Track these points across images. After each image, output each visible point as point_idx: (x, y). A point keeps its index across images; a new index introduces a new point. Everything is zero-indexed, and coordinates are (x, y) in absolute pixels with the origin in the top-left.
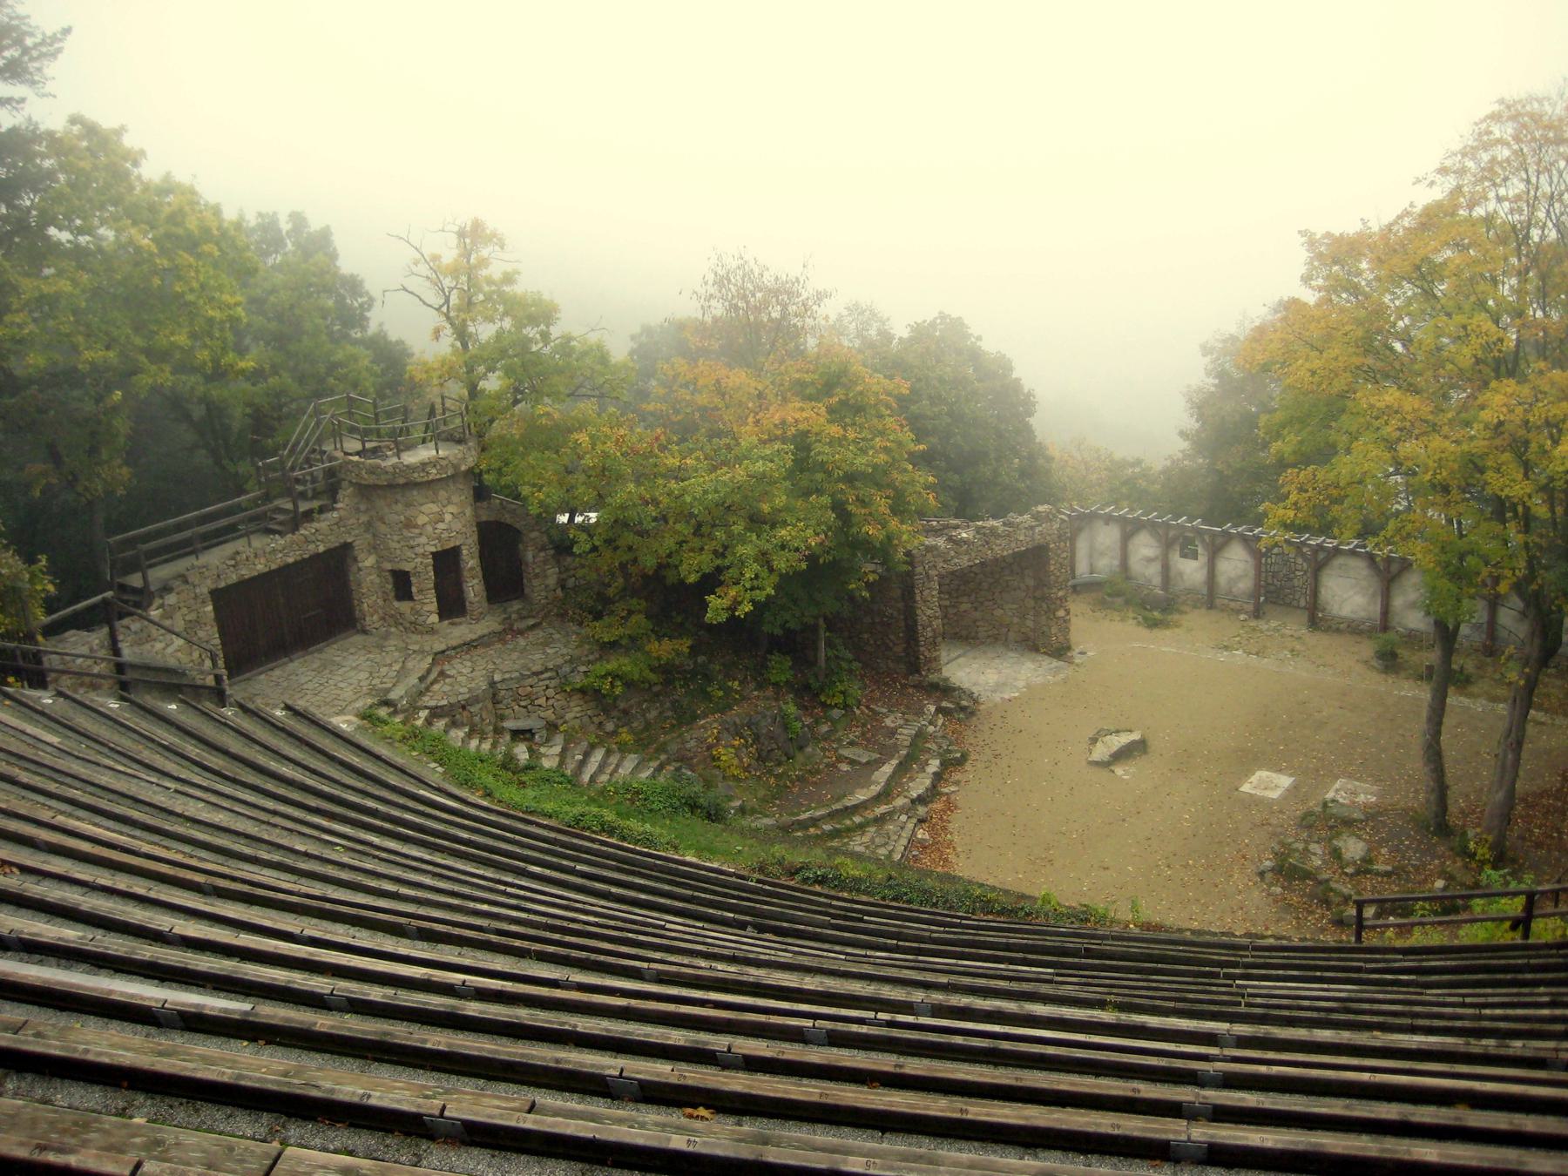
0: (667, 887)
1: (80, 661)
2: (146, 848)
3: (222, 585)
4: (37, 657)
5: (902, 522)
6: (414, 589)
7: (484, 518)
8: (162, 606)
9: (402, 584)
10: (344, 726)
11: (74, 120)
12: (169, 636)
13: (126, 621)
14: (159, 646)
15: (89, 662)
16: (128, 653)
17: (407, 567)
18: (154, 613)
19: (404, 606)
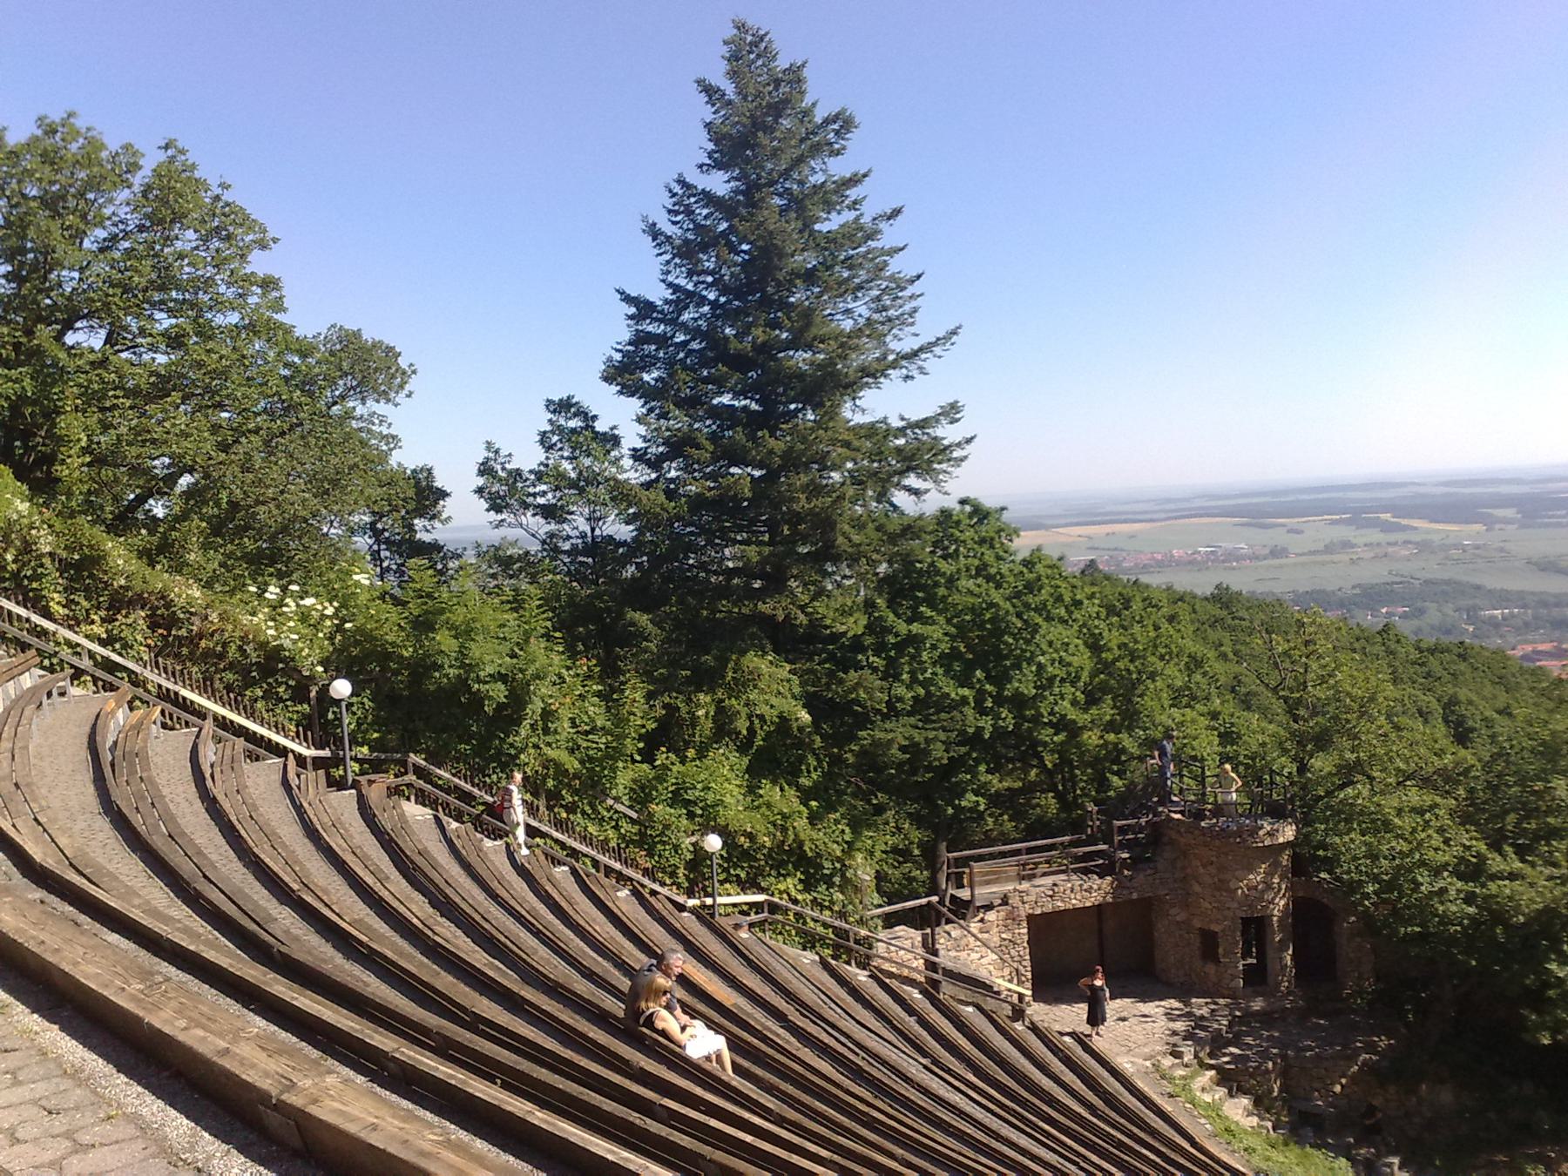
0: (1144, 1151)
1: (902, 952)
2: (910, 1122)
3: (1038, 911)
4: (867, 943)
5: (911, 748)
6: (1221, 950)
7: (1301, 894)
8: (982, 920)
9: (1209, 945)
10: (1128, 1066)
11: (963, 502)
12: (984, 949)
13: (947, 927)
14: (975, 956)
15: (910, 956)
16: (945, 959)
17: (1216, 928)
18: (974, 926)
19: (1211, 969)
